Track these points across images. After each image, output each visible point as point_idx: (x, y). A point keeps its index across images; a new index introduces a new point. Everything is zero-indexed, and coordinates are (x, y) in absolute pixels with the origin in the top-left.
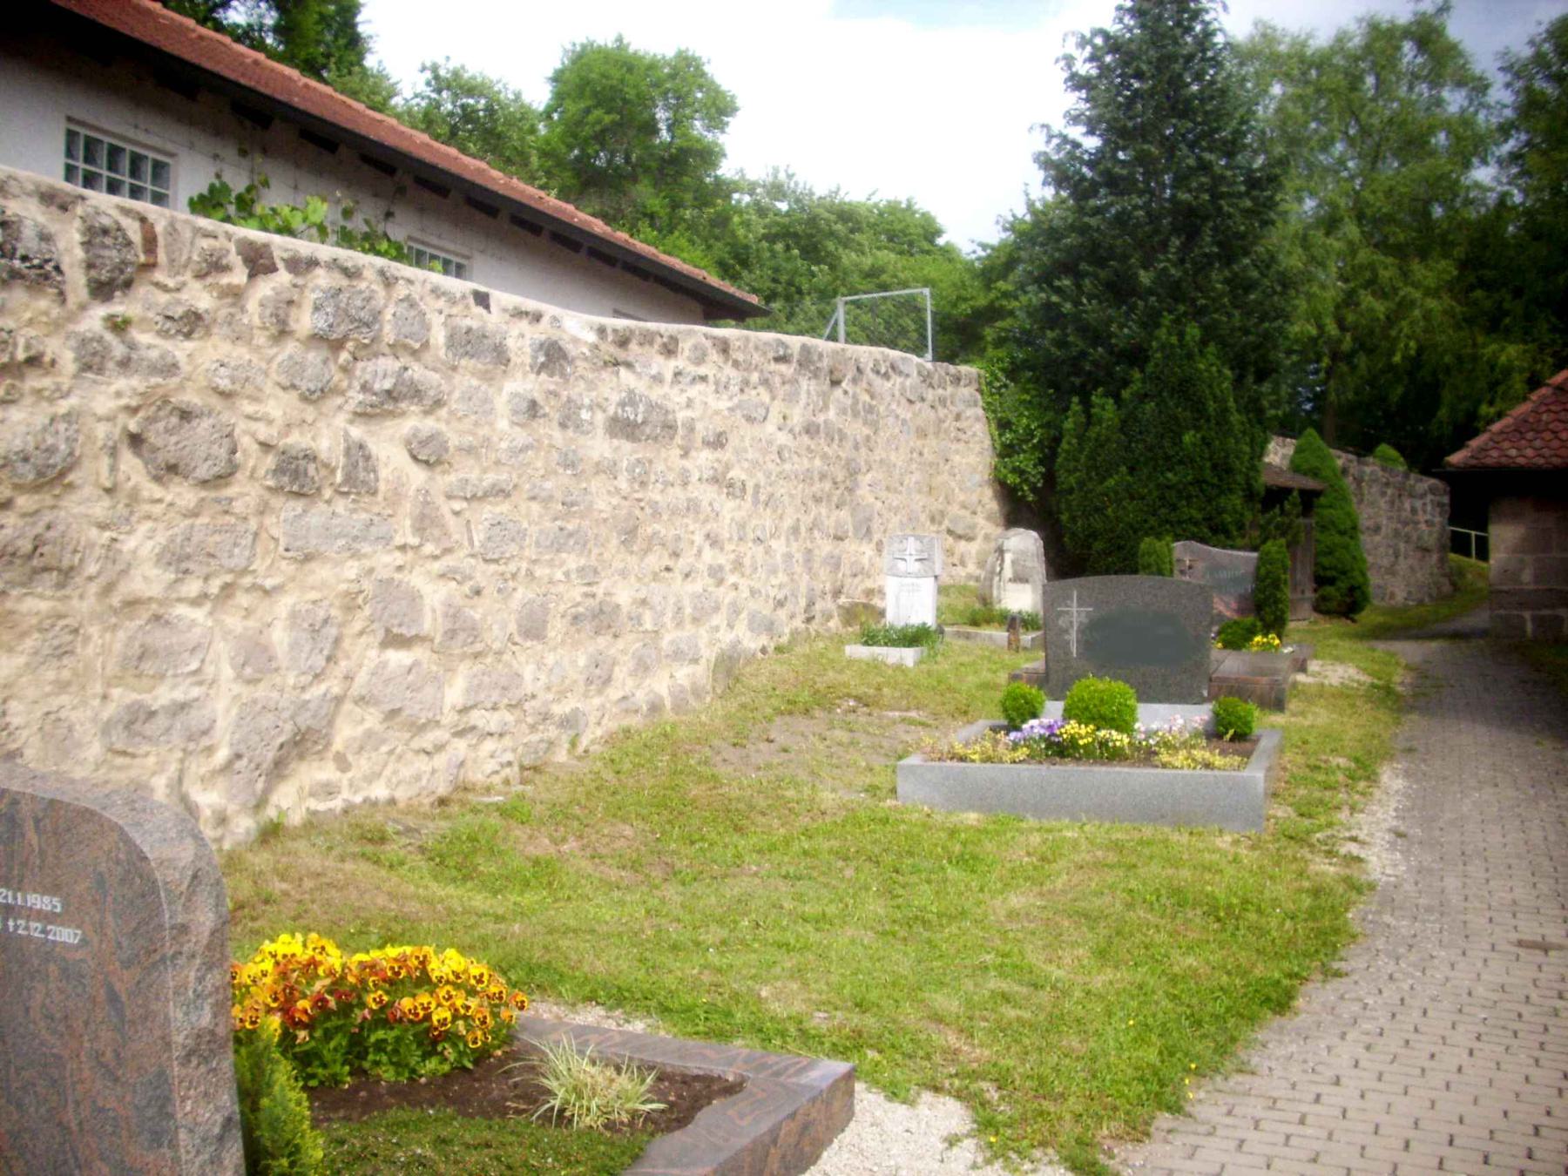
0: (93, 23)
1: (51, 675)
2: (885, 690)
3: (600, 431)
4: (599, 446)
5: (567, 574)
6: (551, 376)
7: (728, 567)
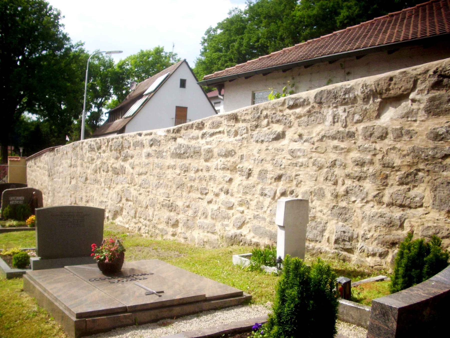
0: (79, 207)
1: (347, 216)
2: (207, 246)
3: (169, 157)
4: (170, 161)
5: (160, 194)
6: (155, 146)
7: (236, 203)
